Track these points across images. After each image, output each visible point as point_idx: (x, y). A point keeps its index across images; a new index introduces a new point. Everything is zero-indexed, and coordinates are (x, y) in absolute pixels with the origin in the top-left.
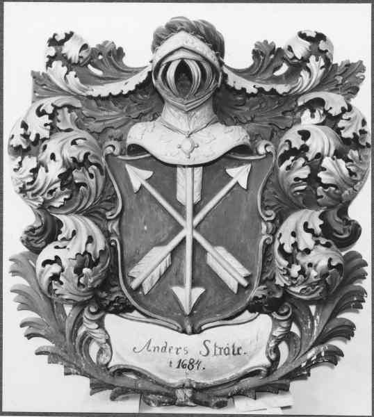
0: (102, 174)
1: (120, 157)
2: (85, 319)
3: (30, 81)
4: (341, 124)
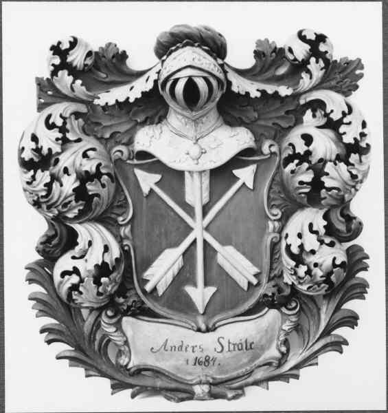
0: (113, 182)
1: (128, 162)
2: (103, 323)
3: (33, 90)
4: (342, 129)
